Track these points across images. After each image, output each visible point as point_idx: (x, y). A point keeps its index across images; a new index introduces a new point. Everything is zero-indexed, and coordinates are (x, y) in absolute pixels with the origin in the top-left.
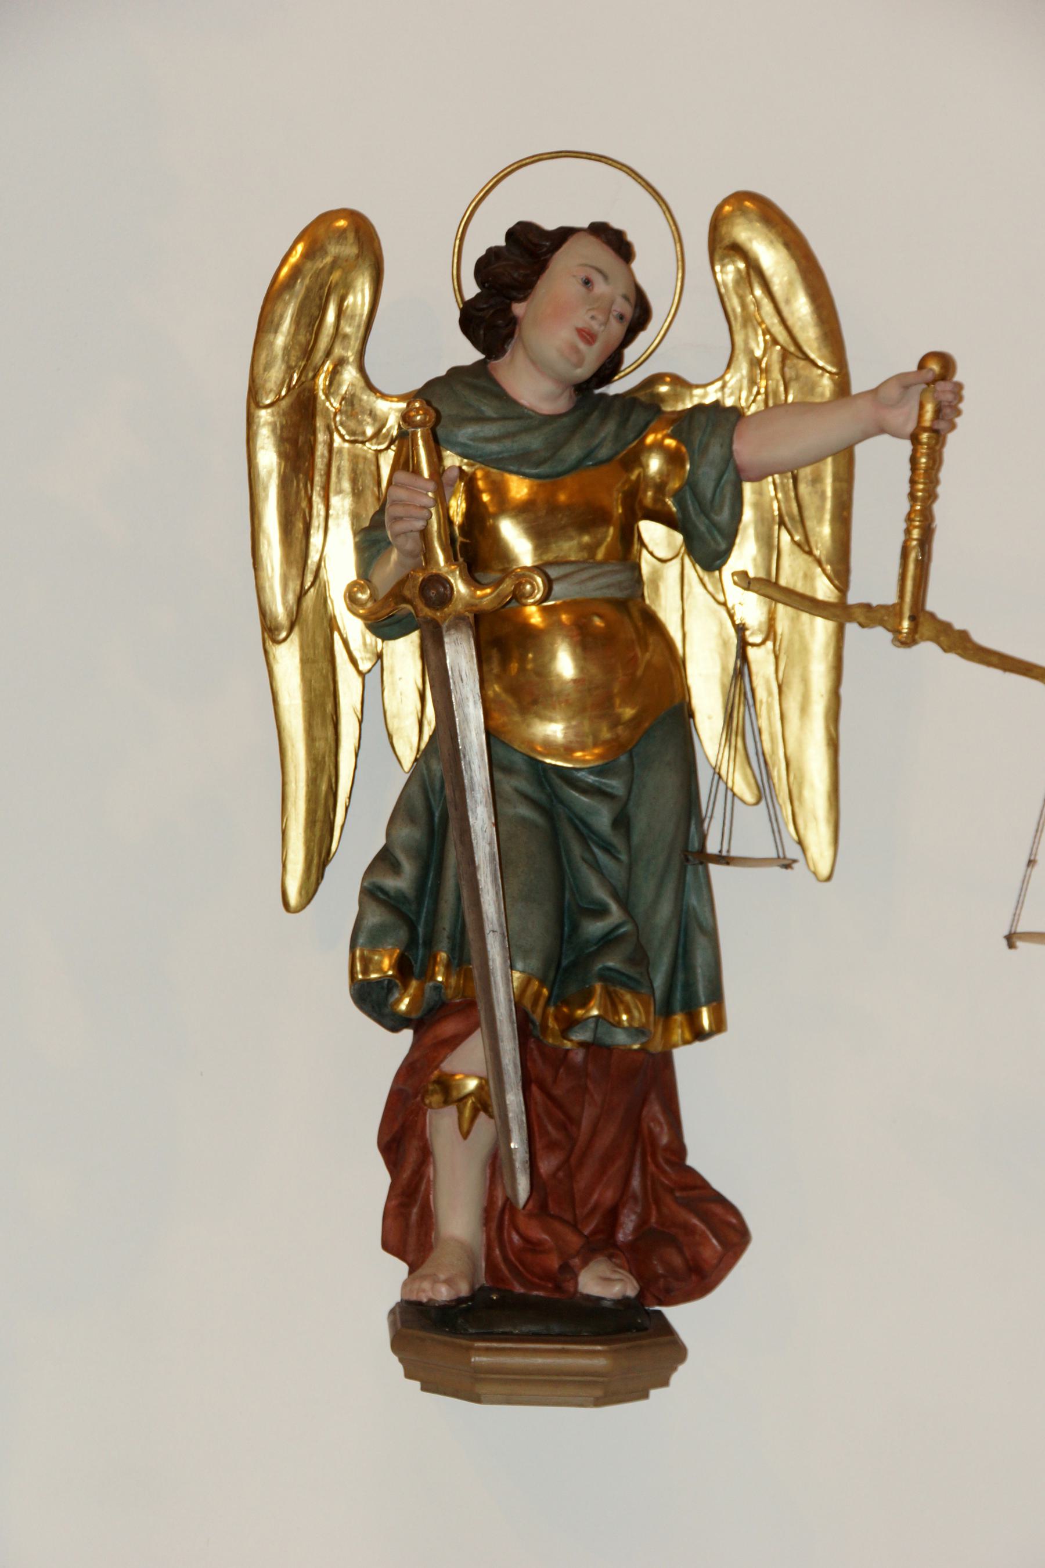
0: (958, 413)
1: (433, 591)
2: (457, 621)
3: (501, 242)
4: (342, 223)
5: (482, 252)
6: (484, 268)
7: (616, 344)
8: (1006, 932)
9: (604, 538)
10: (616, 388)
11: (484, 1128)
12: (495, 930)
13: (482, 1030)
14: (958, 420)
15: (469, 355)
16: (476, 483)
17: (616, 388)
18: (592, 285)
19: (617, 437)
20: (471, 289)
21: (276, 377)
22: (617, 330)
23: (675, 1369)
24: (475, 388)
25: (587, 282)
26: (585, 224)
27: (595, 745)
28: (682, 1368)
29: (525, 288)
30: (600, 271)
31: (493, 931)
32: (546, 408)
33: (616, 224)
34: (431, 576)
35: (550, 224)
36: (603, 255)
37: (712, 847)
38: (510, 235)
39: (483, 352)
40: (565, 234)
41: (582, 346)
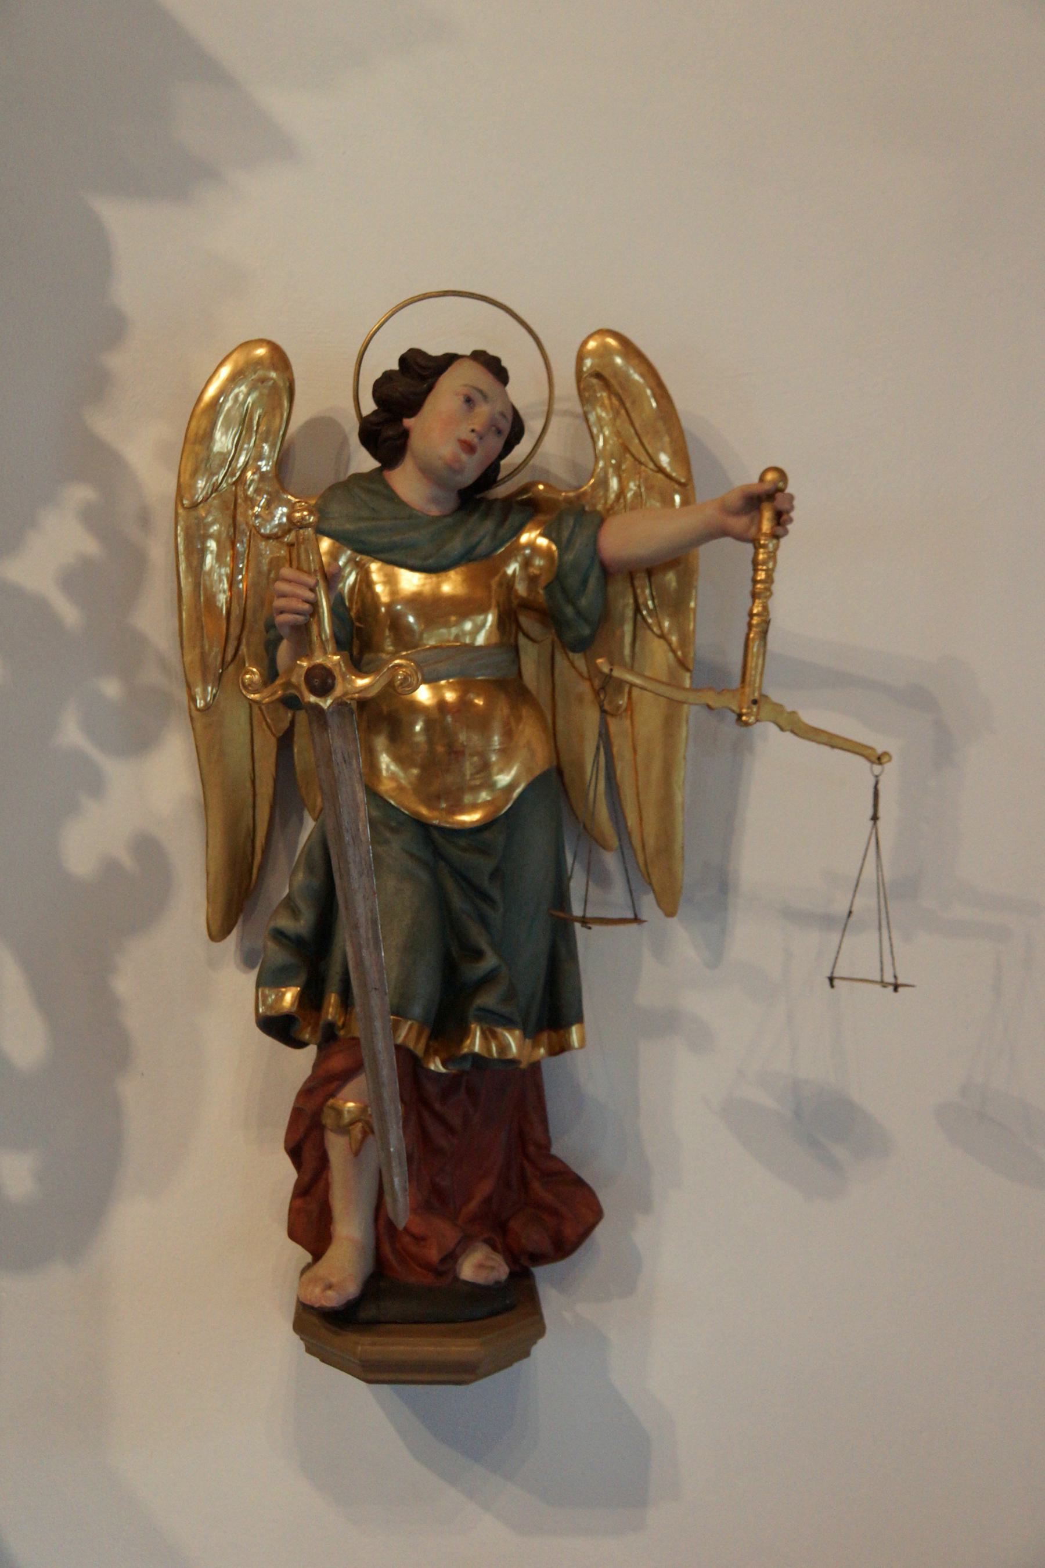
0: (791, 520)
1: (316, 680)
2: (340, 707)
3: (395, 366)
4: (261, 351)
5: (379, 375)
6: (383, 387)
7: (494, 456)
8: (829, 975)
9: (483, 625)
10: (501, 491)
11: (372, 1150)
12: (377, 987)
13: (366, 1075)
14: (789, 527)
15: (365, 462)
16: (371, 577)
17: (501, 491)
18: (474, 406)
19: (494, 535)
20: (369, 406)
21: (586, 490)
22: (497, 443)
23: (535, 1343)
24: (369, 491)
25: (468, 400)
26: (468, 353)
27: (406, 1229)
28: (541, 1342)
29: (414, 405)
30: (481, 392)
31: (376, 989)
32: (434, 511)
33: (492, 351)
34: (306, 674)
35: (435, 349)
36: (482, 378)
37: (577, 910)
38: (403, 360)
39: (380, 461)
40: (449, 360)
41: (464, 457)
